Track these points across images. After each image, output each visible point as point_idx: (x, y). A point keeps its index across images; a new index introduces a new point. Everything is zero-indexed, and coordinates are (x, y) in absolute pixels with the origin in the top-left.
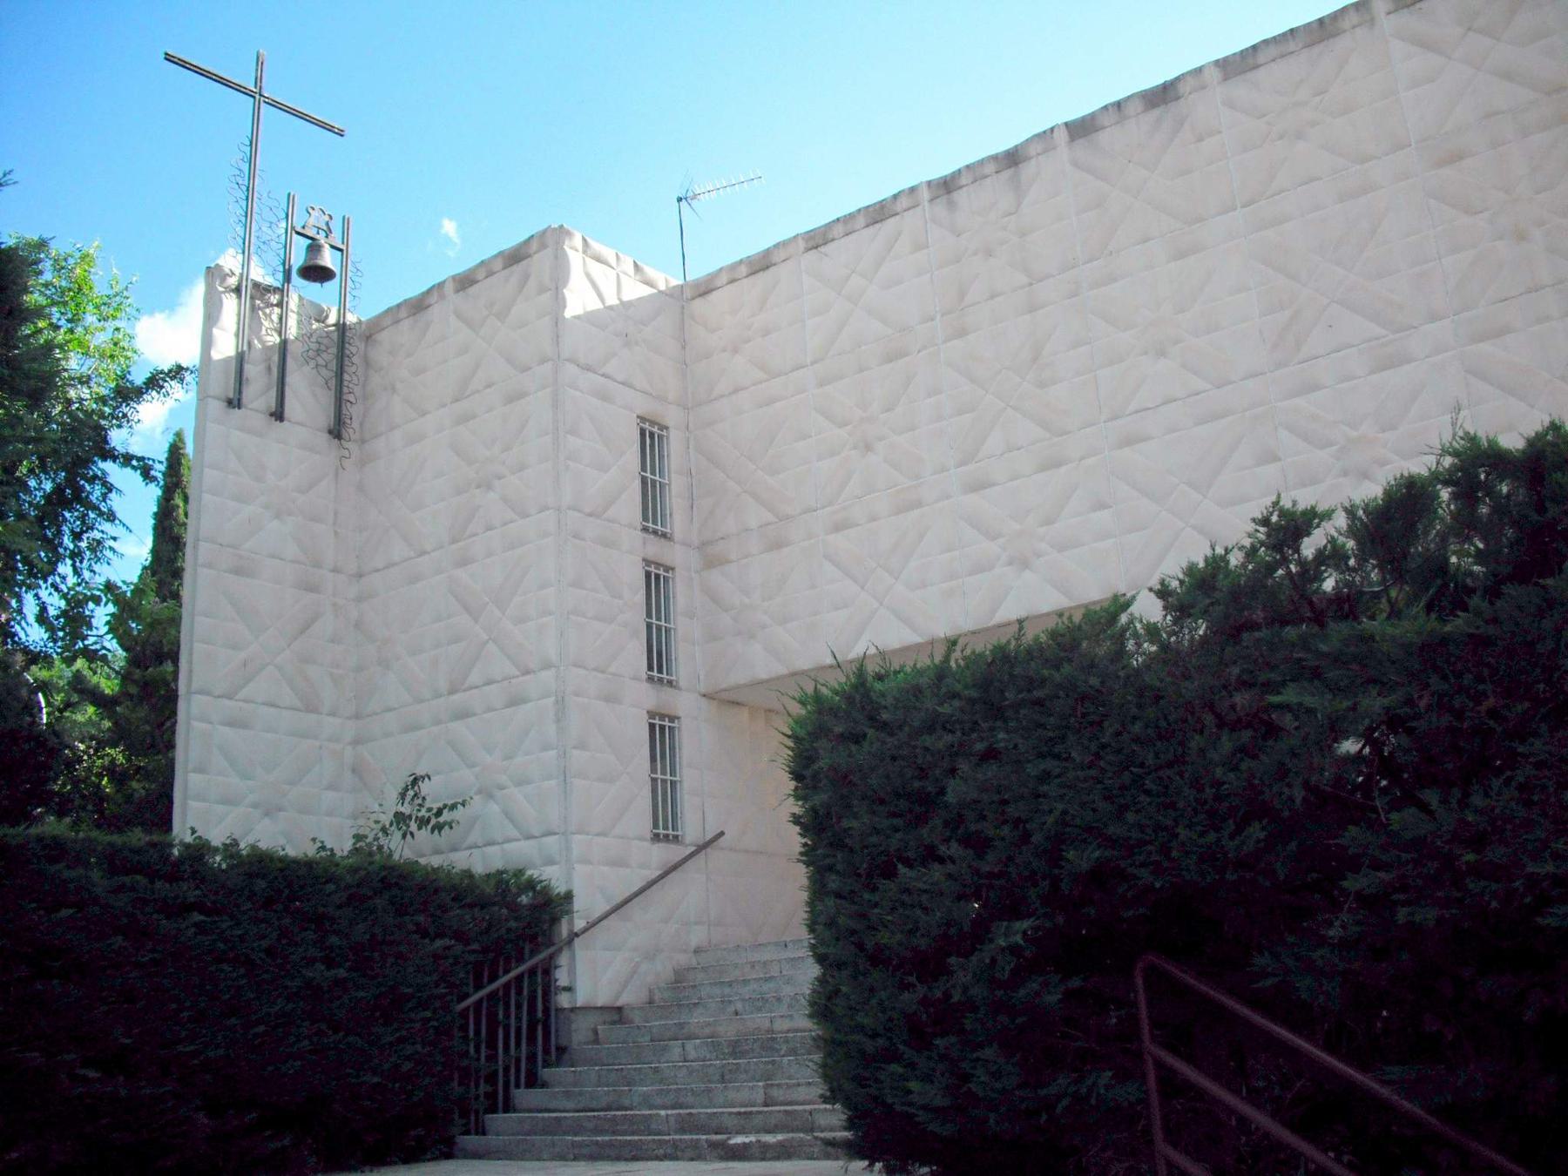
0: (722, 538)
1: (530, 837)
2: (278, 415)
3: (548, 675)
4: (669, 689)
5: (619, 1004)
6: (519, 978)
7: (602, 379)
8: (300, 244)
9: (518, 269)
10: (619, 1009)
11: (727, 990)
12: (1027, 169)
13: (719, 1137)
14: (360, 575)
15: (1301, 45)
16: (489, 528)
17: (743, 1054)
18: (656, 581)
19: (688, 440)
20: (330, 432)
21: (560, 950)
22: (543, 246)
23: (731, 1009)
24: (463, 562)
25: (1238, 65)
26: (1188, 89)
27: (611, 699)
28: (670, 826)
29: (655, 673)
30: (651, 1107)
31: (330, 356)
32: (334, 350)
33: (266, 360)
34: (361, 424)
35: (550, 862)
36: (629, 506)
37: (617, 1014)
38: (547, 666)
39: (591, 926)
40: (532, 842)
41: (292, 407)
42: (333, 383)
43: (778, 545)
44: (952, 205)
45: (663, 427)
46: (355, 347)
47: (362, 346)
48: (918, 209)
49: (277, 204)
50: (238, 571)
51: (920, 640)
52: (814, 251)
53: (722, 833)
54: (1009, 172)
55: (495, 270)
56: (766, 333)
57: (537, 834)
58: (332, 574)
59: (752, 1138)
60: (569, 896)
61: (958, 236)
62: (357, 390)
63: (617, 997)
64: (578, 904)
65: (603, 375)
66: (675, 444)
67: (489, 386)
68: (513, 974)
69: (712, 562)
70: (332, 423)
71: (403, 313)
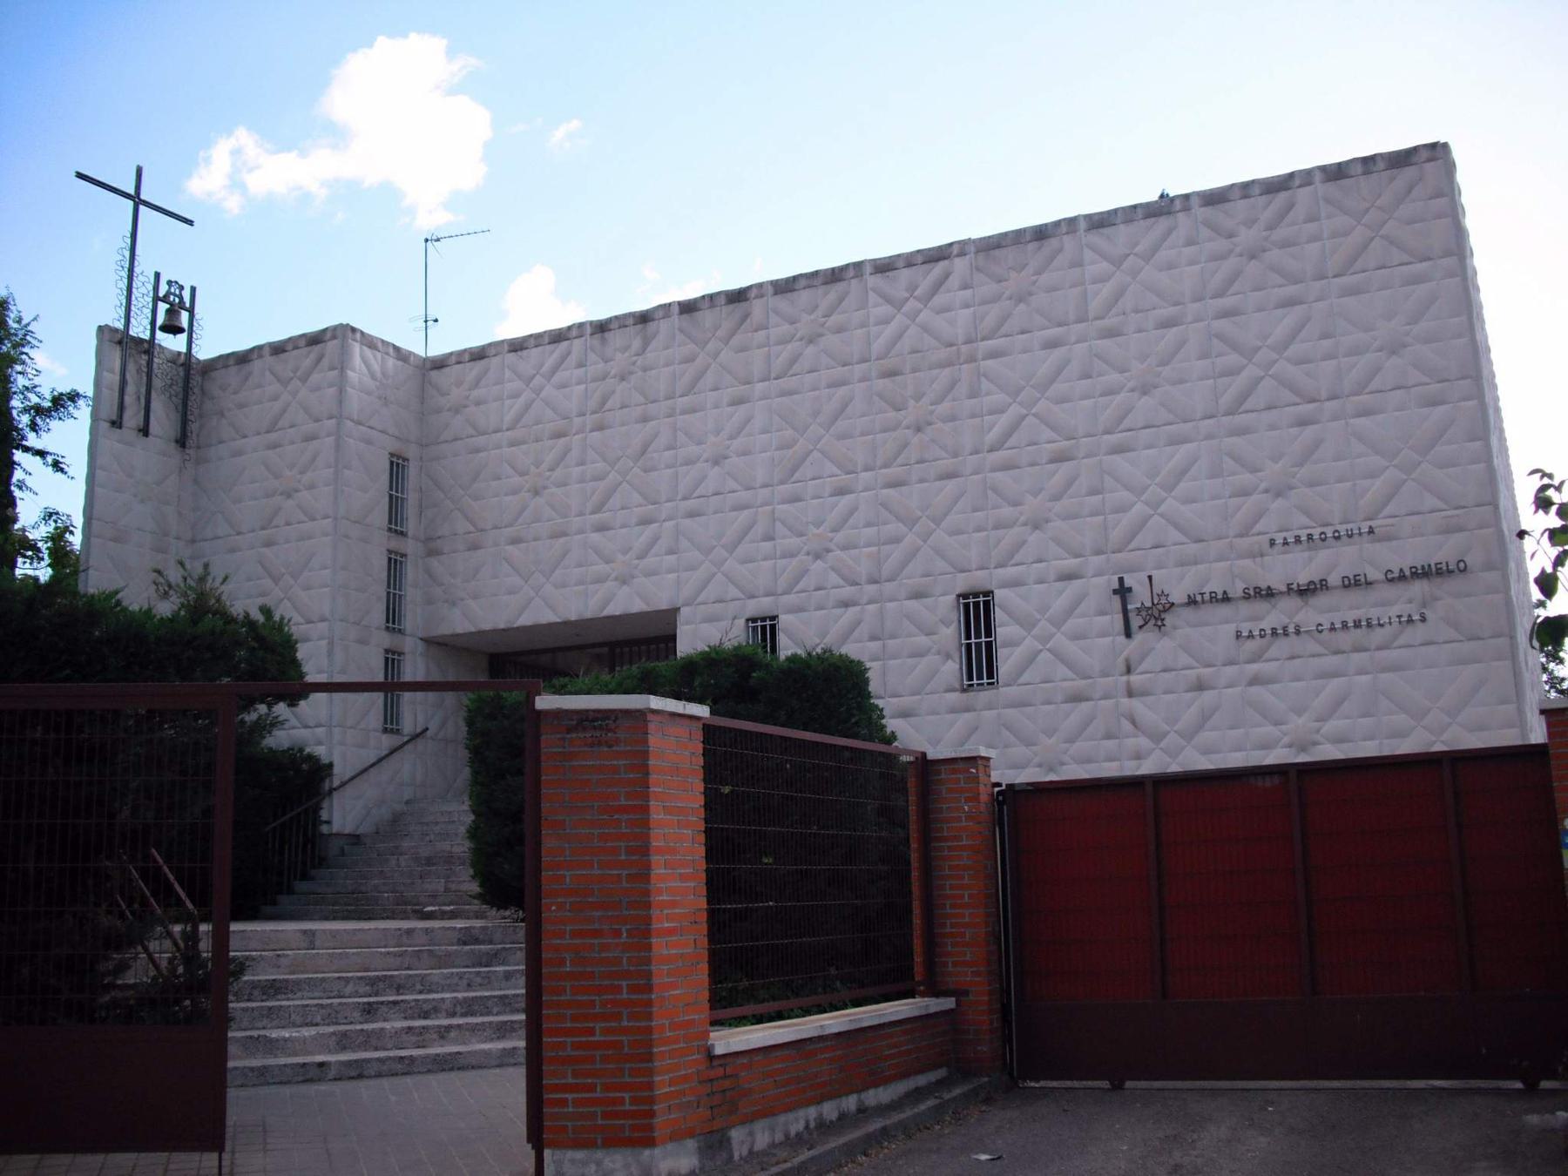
0: (439, 537)
1: (306, 727)
2: (145, 431)
3: (323, 626)
4: (400, 635)
5: (358, 833)
6: (299, 814)
7: (369, 430)
8: (163, 307)
9: (317, 348)
10: (358, 837)
11: (425, 828)
12: (652, 326)
13: (417, 907)
14: (193, 541)
15: (820, 282)
16: (288, 524)
17: (434, 864)
18: (395, 564)
19: (421, 467)
20: (177, 441)
21: (324, 798)
22: (334, 337)
23: (428, 838)
24: (269, 544)
25: (785, 287)
26: (753, 295)
27: (363, 641)
28: (389, 721)
29: (390, 625)
30: (379, 892)
31: (178, 388)
32: (181, 385)
33: (136, 393)
34: (198, 435)
35: (320, 743)
36: (380, 516)
37: (355, 839)
38: (323, 620)
39: (343, 784)
40: (310, 730)
41: (154, 427)
42: (180, 408)
43: (475, 547)
44: (604, 341)
45: (405, 460)
46: (196, 380)
47: (199, 379)
48: (583, 339)
49: (147, 280)
50: (116, 540)
51: (558, 620)
52: (513, 353)
53: (427, 729)
54: (640, 326)
55: (300, 346)
56: (478, 403)
57: (311, 725)
58: (175, 540)
59: (437, 908)
60: (331, 765)
61: (606, 362)
62: (196, 412)
63: (358, 827)
64: (336, 770)
65: (369, 427)
66: (412, 471)
67: (291, 427)
68: (294, 813)
69: (433, 553)
70: (179, 435)
71: (231, 362)
